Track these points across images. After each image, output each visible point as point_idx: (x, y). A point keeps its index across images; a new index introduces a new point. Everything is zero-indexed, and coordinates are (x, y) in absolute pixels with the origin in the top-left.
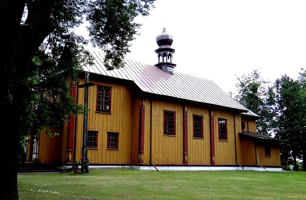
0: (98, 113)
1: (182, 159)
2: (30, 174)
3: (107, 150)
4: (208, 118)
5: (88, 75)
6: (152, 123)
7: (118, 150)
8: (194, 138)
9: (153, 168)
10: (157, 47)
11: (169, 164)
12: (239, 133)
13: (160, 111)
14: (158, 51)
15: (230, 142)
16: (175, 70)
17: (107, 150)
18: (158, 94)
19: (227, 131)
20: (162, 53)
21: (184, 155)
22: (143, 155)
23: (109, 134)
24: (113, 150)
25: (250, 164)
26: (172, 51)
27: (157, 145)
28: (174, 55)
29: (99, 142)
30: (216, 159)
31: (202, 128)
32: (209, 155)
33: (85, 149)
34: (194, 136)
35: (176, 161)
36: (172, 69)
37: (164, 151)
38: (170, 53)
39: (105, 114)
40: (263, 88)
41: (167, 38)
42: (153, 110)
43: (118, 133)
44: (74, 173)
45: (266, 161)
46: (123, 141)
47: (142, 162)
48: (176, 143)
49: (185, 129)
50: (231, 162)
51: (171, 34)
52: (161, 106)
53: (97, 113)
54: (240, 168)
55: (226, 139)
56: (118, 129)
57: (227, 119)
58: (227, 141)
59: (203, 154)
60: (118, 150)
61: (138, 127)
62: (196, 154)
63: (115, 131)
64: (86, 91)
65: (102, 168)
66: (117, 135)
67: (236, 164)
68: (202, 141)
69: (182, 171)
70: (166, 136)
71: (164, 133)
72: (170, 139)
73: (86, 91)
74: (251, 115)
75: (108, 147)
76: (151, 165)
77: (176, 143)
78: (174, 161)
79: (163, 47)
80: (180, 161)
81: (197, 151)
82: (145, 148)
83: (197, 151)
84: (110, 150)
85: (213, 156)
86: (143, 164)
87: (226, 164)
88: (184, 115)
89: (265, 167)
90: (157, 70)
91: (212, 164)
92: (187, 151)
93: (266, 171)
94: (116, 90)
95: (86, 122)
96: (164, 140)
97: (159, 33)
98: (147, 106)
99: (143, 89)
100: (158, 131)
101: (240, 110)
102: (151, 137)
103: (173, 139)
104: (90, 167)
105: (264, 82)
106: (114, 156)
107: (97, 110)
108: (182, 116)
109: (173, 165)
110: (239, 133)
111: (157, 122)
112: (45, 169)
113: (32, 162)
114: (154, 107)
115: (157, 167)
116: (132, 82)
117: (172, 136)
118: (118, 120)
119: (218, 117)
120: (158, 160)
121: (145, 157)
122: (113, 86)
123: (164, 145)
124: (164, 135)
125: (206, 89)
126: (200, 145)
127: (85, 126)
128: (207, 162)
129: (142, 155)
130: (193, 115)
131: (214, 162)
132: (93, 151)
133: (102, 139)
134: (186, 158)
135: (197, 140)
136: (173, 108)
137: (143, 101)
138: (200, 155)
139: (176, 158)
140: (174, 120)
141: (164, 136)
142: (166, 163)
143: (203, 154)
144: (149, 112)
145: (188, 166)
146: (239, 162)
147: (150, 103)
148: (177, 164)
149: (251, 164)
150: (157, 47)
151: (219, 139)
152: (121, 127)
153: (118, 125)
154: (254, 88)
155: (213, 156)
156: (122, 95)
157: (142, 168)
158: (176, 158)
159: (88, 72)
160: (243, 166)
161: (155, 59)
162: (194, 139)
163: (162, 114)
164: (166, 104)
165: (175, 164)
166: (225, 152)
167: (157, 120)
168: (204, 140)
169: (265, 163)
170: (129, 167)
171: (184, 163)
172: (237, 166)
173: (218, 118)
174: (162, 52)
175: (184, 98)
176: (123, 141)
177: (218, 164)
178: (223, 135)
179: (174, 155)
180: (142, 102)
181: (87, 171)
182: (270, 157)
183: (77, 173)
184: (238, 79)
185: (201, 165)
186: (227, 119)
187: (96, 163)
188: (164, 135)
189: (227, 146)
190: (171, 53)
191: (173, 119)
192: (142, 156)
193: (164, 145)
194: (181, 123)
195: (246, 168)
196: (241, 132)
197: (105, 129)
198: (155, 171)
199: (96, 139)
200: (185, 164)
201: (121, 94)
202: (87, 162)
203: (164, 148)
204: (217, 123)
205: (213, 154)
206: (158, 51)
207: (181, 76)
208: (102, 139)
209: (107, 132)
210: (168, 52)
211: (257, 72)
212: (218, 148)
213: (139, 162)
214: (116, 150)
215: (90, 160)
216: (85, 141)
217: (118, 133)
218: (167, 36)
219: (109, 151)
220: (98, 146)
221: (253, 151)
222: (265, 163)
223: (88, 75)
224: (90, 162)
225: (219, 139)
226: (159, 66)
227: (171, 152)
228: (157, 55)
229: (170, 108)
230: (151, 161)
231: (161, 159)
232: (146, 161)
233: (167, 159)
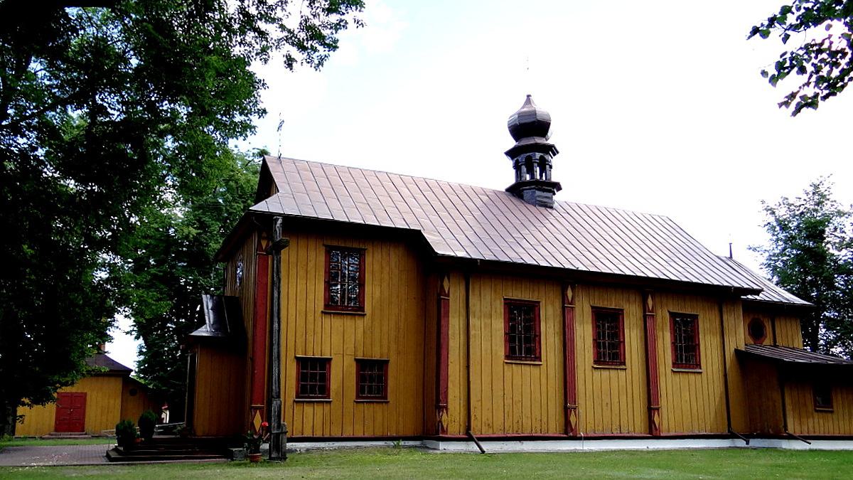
0: (330, 314)
1: (562, 420)
2: (144, 464)
3: (357, 402)
4: (639, 314)
5: (280, 221)
6: (472, 332)
7: (327, 402)
8: (595, 366)
9: (473, 447)
10: (511, 143)
11: (522, 435)
12: (737, 351)
13: (495, 301)
14: (511, 153)
15: (710, 373)
16: (558, 197)
17: (357, 402)
18: (480, 259)
19: (699, 345)
20: (522, 158)
21: (566, 411)
22: (447, 413)
23: (362, 365)
24: (303, 402)
25: (768, 431)
26: (551, 150)
27: (486, 387)
28: (555, 161)
29: (334, 384)
30: (665, 420)
31: (622, 340)
32: (560, 410)
33: (275, 402)
34: (595, 362)
35: (544, 426)
36: (549, 195)
37: (508, 402)
38: (541, 156)
39: (349, 317)
40: (838, 230)
41: (534, 120)
42: (725, 317)
43: (387, 362)
44: (249, 461)
45: (817, 423)
46: (400, 381)
47: (444, 431)
48: (544, 381)
49: (568, 344)
50: (708, 428)
51: (542, 107)
52: (498, 290)
53: (325, 313)
54: (741, 443)
55: (699, 366)
56: (385, 351)
57: (539, 302)
58: (624, 367)
59: (623, 407)
60: (330, 402)
61: (434, 345)
62: (605, 408)
63: (377, 357)
64: (275, 262)
65: (340, 449)
66: (382, 365)
67: (729, 431)
68: (622, 374)
69: (558, 454)
70: (512, 363)
71: (594, 361)
72: (523, 374)
73: (275, 262)
74: (782, 302)
75: (358, 397)
76: (469, 438)
77: (544, 381)
78: (538, 426)
79: (525, 142)
80: (554, 427)
81: (606, 400)
82: (450, 397)
83: (606, 400)
84: (363, 402)
85: (656, 413)
86: (449, 436)
87: (697, 433)
88: (564, 308)
89: (805, 438)
90: (514, 203)
91: (653, 432)
92: (575, 402)
93: (811, 451)
94: (378, 256)
95: (277, 337)
96: (508, 374)
97: (512, 108)
98: (455, 292)
99: (440, 250)
100: (489, 351)
101: (736, 288)
102: (468, 367)
103: (535, 371)
104: (289, 445)
105: (840, 214)
106: (374, 416)
107: (326, 306)
108: (559, 311)
109: (534, 437)
110: (737, 351)
111: (485, 330)
112: (197, 453)
113: (173, 436)
114: (477, 292)
115: (481, 444)
116: (418, 234)
117: (530, 365)
118: (385, 328)
119: (669, 311)
120: (491, 425)
121: (452, 418)
122: (370, 249)
123: (508, 386)
124: (506, 361)
125: (642, 237)
126: (614, 384)
127: (275, 347)
128: (637, 429)
129: (445, 415)
130: (592, 307)
131: (447, 429)
132: (319, 409)
133: (342, 376)
134: (572, 419)
135: (605, 373)
136: (534, 291)
137: (444, 278)
138: (616, 408)
139: (545, 419)
140: (535, 321)
141: (506, 367)
142: (515, 432)
143: (623, 407)
144: (463, 305)
145: (580, 439)
146: (737, 425)
147: (464, 283)
148: (547, 435)
149: (770, 430)
150: (511, 143)
151: (673, 367)
152: (393, 346)
153: (385, 342)
154: (815, 230)
155: (656, 413)
156: (396, 267)
157: (442, 446)
158: (545, 419)
159: (280, 215)
160: (747, 437)
161: (506, 175)
162: (595, 368)
163: (500, 309)
164: (510, 283)
165: (541, 435)
166: (694, 403)
167: (485, 324)
168: (628, 371)
169: (814, 428)
170: (418, 443)
171: (566, 432)
172: (731, 435)
173: (670, 313)
174: (522, 156)
175: (632, 274)
176: (400, 381)
177: (672, 434)
178: (687, 356)
179: (537, 413)
180: (442, 282)
181: (283, 458)
182: (832, 412)
183: (257, 462)
184: (770, 212)
185: (620, 435)
186: (539, 302)
187: (327, 435)
188: (506, 363)
189: (699, 385)
190: (546, 157)
191: (617, 327)
192: (444, 417)
193: (508, 386)
194: (557, 330)
195: (754, 443)
196: (742, 348)
197: (350, 350)
198: (476, 453)
199: (325, 379)
200: (569, 433)
201: (393, 264)
202: (282, 433)
203: (509, 395)
204: (666, 324)
205: (573, 406)
206: (511, 153)
207: (567, 210)
208: (342, 376)
209: (356, 360)
210: (538, 155)
211: (822, 189)
212: (670, 392)
213: (437, 433)
214: (382, 402)
215: (289, 429)
216: (276, 384)
217: (387, 362)
218: (533, 115)
219: (362, 405)
220: (332, 394)
221: (777, 396)
222: (814, 428)
223: (280, 221)
224: (288, 435)
225: (673, 367)
226: (516, 191)
227: (527, 403)
228: (509, 163)
229: (522, 294)
230: (468, 428)
231: (498, 423)
232: (454, 427)
233: (515, 421)
